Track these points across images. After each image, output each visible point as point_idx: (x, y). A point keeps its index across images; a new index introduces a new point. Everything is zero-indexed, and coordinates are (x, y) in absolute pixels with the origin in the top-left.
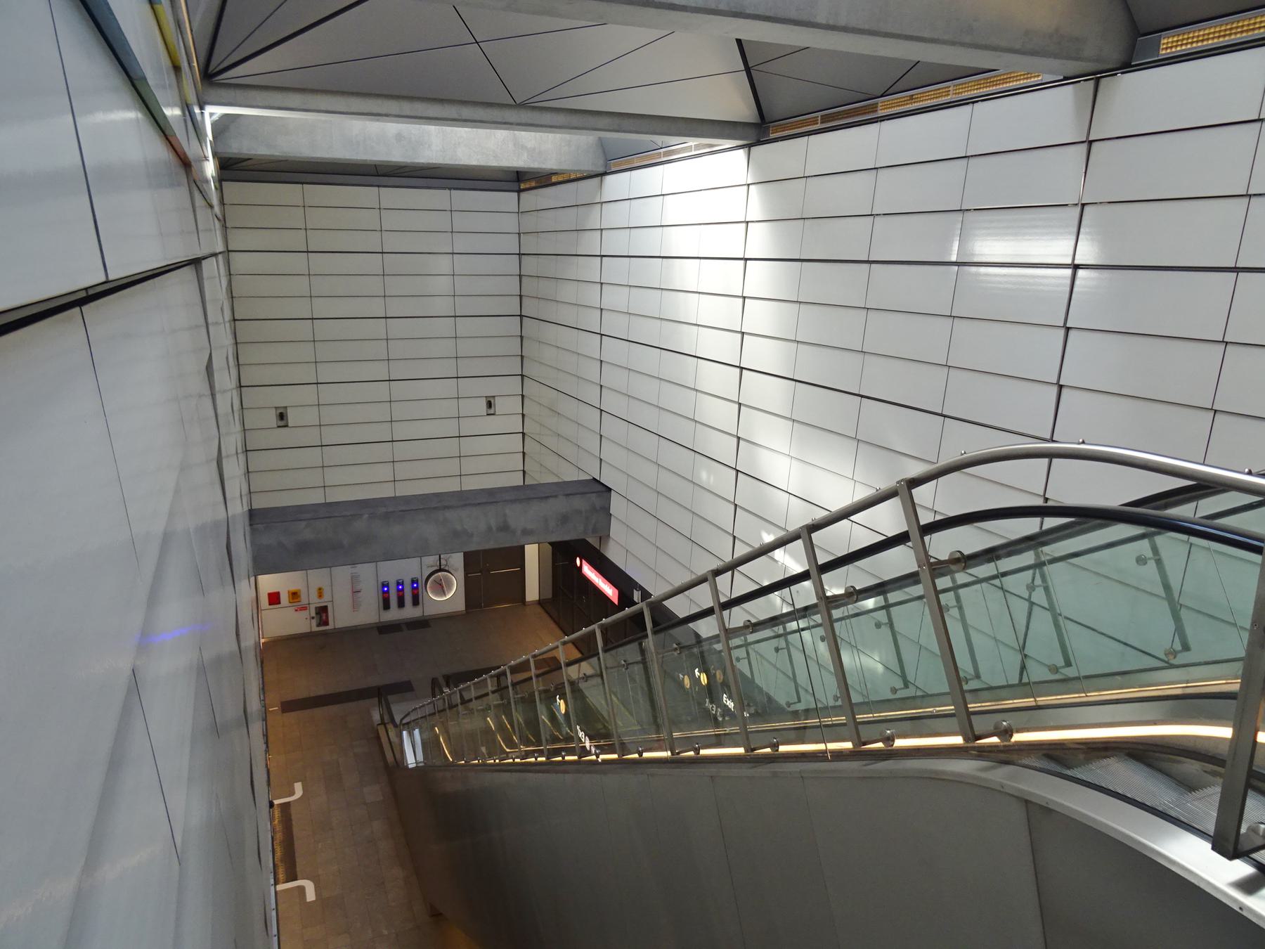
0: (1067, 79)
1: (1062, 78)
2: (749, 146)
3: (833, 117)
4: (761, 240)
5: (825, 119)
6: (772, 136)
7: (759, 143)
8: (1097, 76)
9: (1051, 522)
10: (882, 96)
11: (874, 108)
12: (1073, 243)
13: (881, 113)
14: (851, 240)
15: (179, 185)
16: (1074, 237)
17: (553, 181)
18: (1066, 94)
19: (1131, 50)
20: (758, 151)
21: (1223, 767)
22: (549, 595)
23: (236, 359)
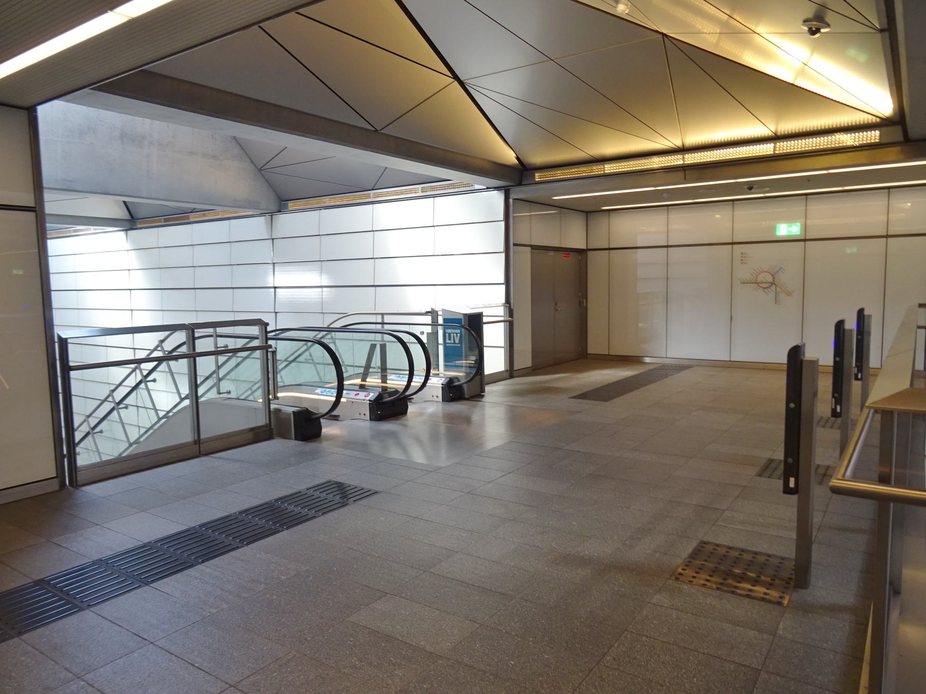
0: (261, 215)
1: (485, 187)
2: (126, 230)
3: (434, 188)
4: (140, 279)
5: (165, 220)
6: (139, 226)
7: (132, 229)
8: (272, 214)
9: (277, 332)
10: (191, 212)
11: (188, 218)
12: (887, 202)
13: (192, 220)
14: (184, 278)
15: (779, 479)
16: (887, 199)
17: (878, 132)
18: (262, 220)
19: (280, 206)
20: (131, 233)
21: (375, 345)
22: (508, 369)
23: (196, 432)
